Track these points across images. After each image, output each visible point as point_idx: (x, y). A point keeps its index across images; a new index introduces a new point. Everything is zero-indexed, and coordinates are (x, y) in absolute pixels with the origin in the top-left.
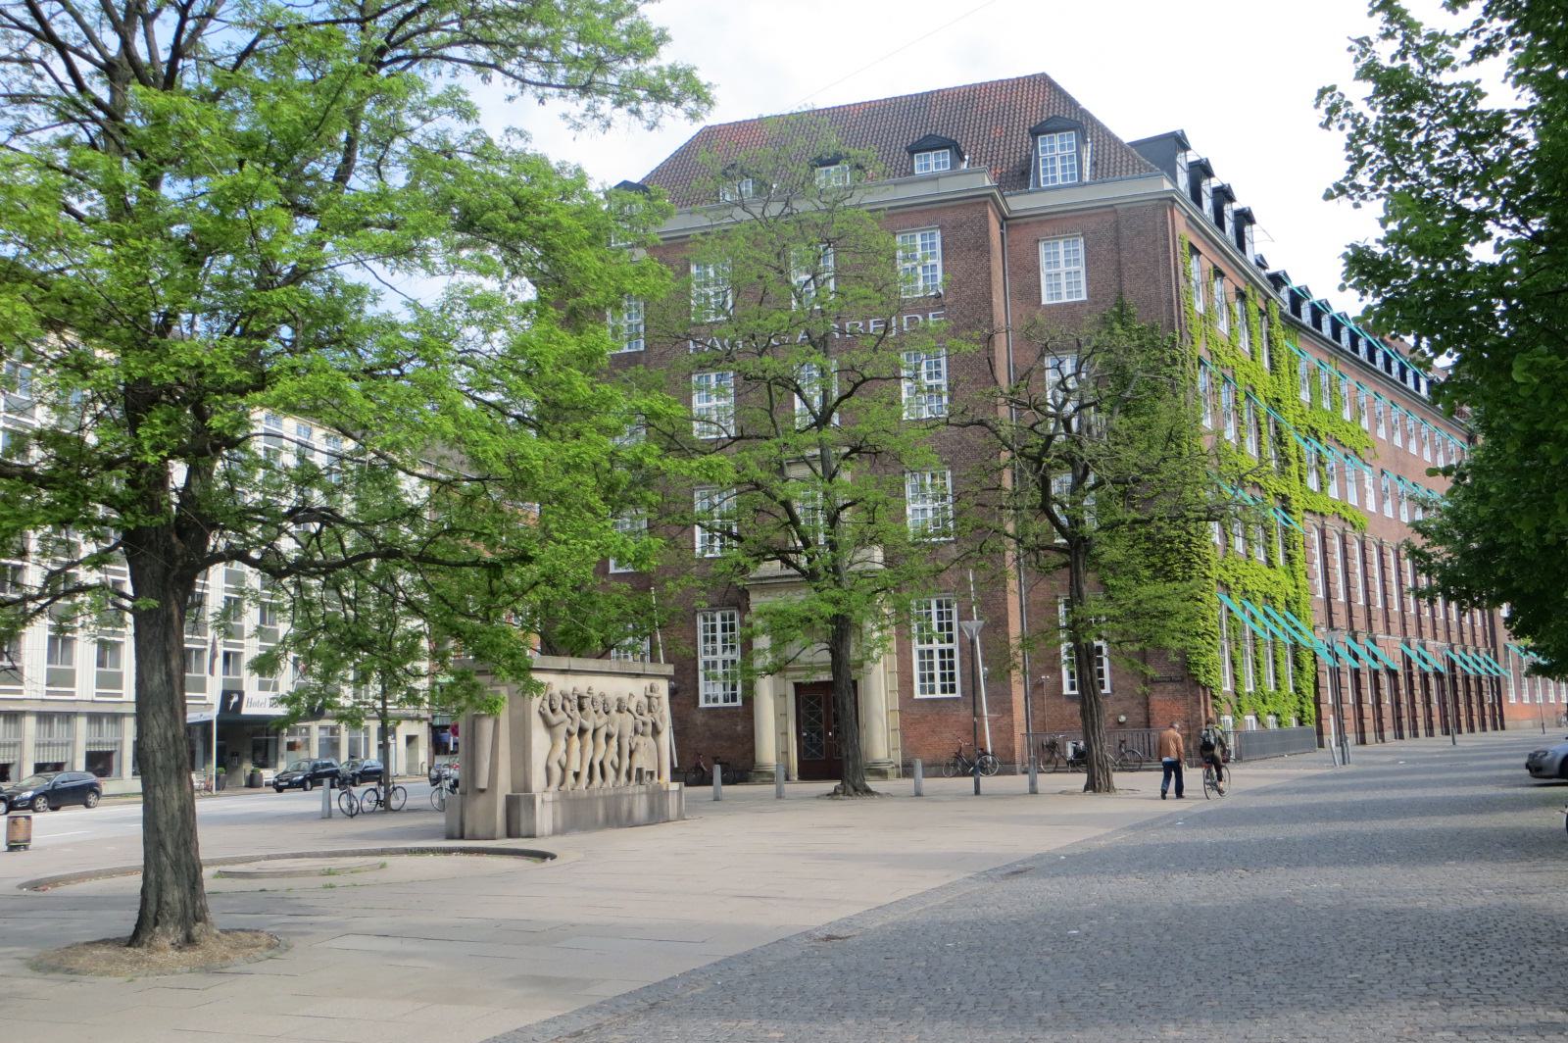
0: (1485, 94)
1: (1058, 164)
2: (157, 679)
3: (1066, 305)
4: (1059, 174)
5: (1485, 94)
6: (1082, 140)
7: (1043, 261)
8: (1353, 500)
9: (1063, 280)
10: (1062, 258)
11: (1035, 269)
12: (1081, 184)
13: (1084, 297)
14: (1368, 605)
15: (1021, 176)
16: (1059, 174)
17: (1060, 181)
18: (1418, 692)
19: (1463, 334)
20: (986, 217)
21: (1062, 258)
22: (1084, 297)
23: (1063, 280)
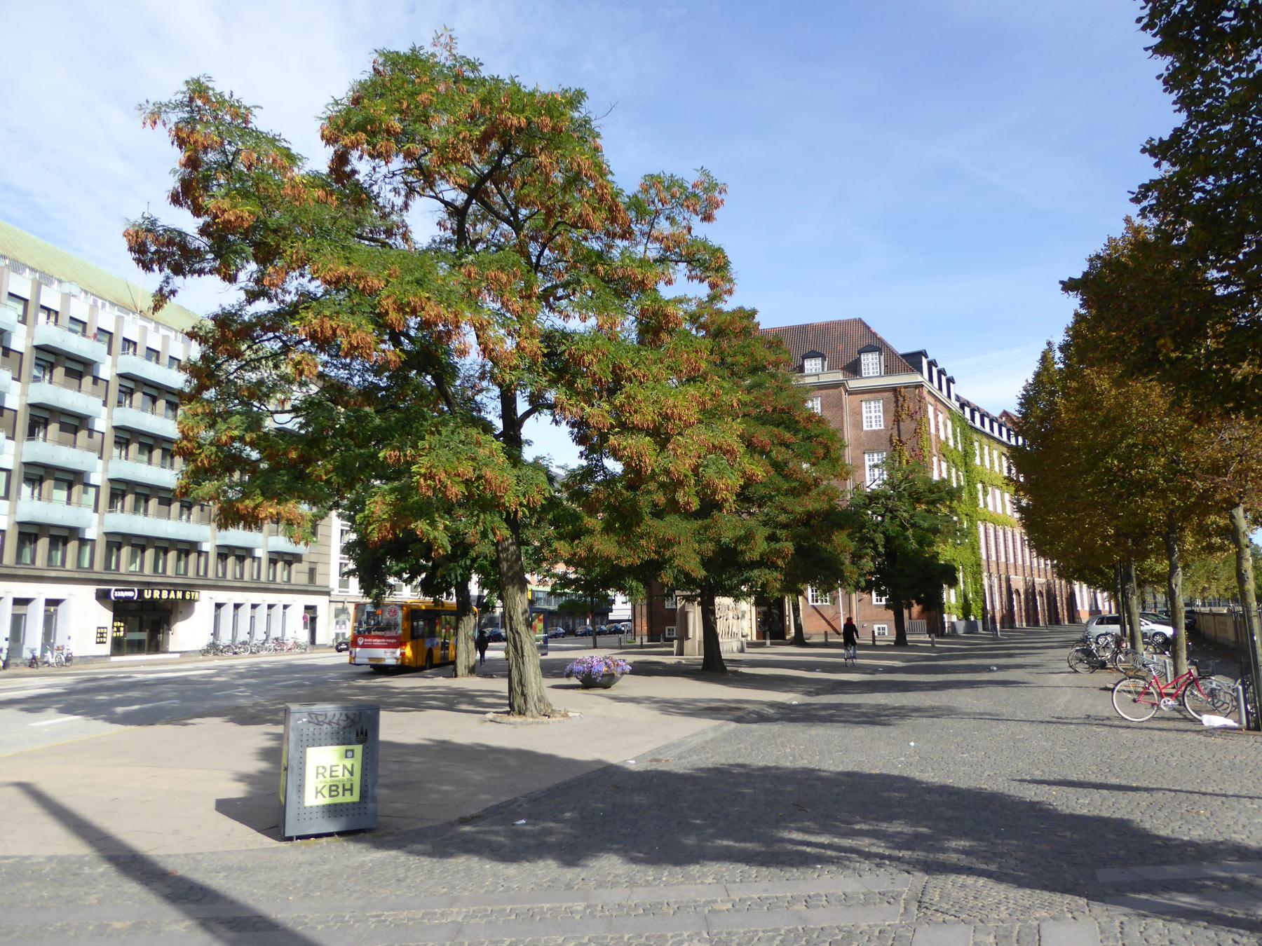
0: (1144, 151)
1: (871, 366)
2: (935, 868)
3: (875, 431)
4: (871, 371)
5: (1144, 151)
6: (880, 354)
7: (864, 410)
8: (991, 508)
9: (873, 419)
10: (873, 409)
11: (861, 414)
12: (880, 376)
13: (883, 427)
14: (988, 558)
15: (854, 369)
16: (871, 371)
17: (871, 374)
18: (1020, 562)
19: (1199, 152)
20: (841, 393)
21: (873, 409)
22: (883, 427)
23: (873, 419)
